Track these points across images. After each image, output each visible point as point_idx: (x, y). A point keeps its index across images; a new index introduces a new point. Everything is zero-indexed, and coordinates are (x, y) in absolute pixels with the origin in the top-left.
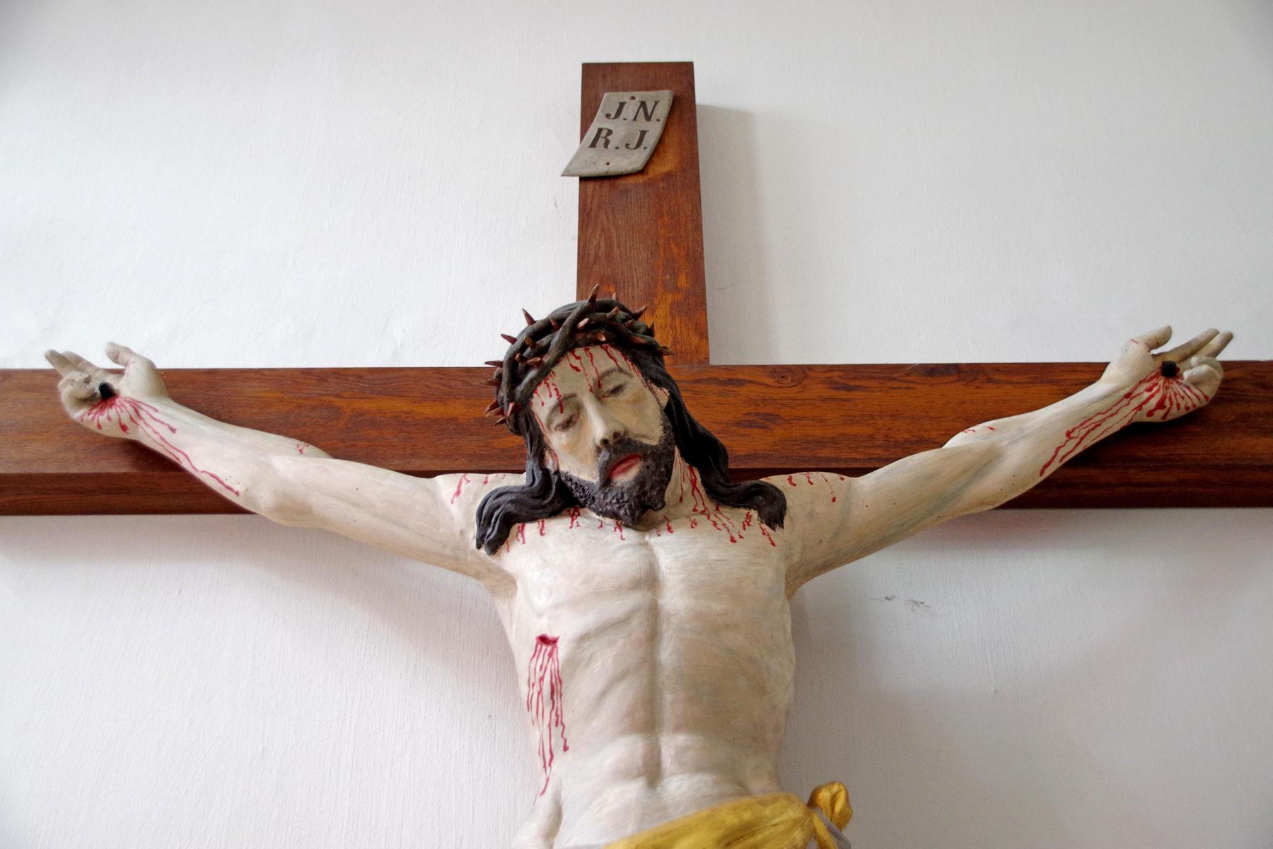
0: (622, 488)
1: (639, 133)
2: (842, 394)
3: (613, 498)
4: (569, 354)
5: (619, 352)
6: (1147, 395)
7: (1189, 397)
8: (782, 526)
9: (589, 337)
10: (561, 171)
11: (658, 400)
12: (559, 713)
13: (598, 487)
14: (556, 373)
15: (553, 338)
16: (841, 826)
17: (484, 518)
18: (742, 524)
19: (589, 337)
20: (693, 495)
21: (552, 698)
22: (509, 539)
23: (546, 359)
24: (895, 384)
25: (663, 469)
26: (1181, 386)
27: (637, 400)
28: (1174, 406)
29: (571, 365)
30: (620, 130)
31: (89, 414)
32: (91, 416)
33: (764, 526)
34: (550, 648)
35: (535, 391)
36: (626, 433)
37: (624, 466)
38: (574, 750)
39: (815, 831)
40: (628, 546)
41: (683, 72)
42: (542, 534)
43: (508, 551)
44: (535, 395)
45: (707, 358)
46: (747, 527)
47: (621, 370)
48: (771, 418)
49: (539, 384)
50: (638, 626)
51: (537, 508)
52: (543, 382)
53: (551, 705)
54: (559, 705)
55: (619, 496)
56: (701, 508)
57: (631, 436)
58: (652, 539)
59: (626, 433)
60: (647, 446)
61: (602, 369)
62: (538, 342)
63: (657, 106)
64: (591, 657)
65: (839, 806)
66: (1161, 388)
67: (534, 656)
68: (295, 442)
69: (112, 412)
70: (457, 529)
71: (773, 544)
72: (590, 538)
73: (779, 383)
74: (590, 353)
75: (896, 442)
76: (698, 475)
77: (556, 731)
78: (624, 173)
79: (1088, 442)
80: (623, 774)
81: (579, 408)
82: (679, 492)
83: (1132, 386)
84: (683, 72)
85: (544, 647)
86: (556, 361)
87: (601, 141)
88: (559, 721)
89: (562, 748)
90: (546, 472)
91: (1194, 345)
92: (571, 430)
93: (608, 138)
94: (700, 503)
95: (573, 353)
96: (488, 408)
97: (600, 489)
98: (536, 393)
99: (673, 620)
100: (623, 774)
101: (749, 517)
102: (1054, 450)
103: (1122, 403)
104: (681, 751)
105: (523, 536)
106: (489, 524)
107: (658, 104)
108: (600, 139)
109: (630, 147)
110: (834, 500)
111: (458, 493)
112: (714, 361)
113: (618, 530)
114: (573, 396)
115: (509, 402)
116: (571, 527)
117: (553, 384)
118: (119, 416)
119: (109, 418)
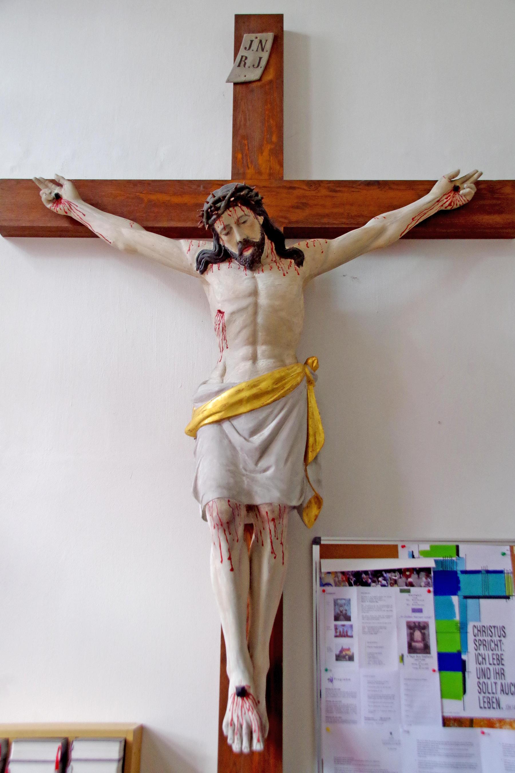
0: (246, 257)
1: (259, 58)
2: (334, 194)
3: (243, 260)
4: (227, 210)
5: (245, 207)
6: (445, 200)
7: (461, 201)
8: (302, 266)
9: (234, 204)
10: (226, 79)
11: (259, 222)
12: (225, 336)
13: (238, 255)
14: (223, 217)
15: (222, 204)
16: (314, 371)
17: (199, 262)
18: (288, 266)
19: (234, 204)
20: (272, 254)
21: (223, 331)
22: (207, 270)
23: (220, 212)
24: (353, 189)
25: (260, 251)
26: (459, 196)
27: (252, 226)
28: (455, 205)
29: (228, 214)
30: (251, 57)
31: (53, 207)
32: (54, 207)
33: (296, 266)
34: (222, 315)
35: (215, 222)
36: (248, 238)
37: (247, 249)
38: (230, 349)
39: (306, 373)
40: (248, 278)
41: (279, 19)
42: (219, 269)
43: (207, 274)
44: (216, 224)
45: (283, 177)
46: (290, 268)
47: (246, 215)
48: (305, 205)
49: (217, 220)
50: (250, 310)
51: (217, 259)
52: (218, 220)
53: (222, 334)
54: (225, 334)
55: (245, 260)
56: (274, 259)
57: (249, 239)
58: (256, 275)
59: (248, 238)
60: (255, 242)
61: (239, 216)
62: (216, 205)
63: (267, 42)
64: (235, 320)
65: (314, 364)
66: (451, 198)
67: (216, 316)
68: (129, 221)
69: (61, 206)
70: (189, 263)
71: (298, 274)
72: (235, 273)
73: (309, 188)
74: (235, 210)
75: (351, 216)
76: (274, 245)
77: (224, 342)
78: (252, 81)
79: (420, 221)
80: (245, 359)
81: (231, 228)
82: (267, 254)
83: (440, 197)
84: (279, 19)
85: (220, 314)
86: (223, 213)
87: (243, 63)
88: (225, 339)
89: (226, 348)
90: (220, 246)
91: (468, 177)
92: (228, 236)
93: (245, 61)
94: (274, 257)
95: (229, 210)
96: (199, 223)
97: (239, 256)
98: (216, 223)
99: (262, 308)
100: (245, 359)
101: (291, 262)
102: (407, 226)
103: (436, 204)
104: (264, 352)
105: (212, 269)
106: (200, 264)
107: (267, 41)
108: (242, 62)
109: (255, 66)
110: (322, 252)
111: (189, 250)
112: (286, 178)
113: (245, 271)
114: (229, 225)
115: (207, 224)
116: (229, 268)
117: (222, 221)
118: (64, 208)
119: (60, 209)
